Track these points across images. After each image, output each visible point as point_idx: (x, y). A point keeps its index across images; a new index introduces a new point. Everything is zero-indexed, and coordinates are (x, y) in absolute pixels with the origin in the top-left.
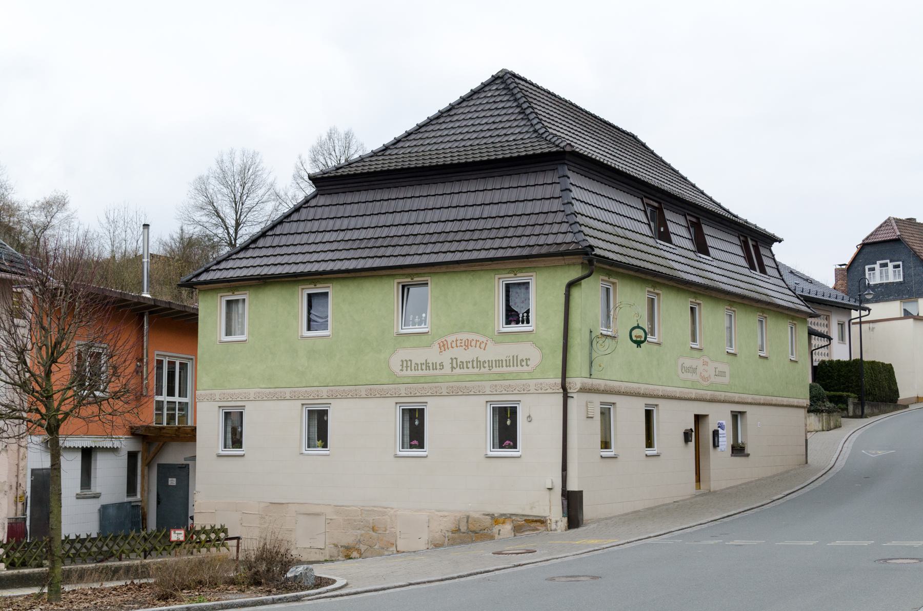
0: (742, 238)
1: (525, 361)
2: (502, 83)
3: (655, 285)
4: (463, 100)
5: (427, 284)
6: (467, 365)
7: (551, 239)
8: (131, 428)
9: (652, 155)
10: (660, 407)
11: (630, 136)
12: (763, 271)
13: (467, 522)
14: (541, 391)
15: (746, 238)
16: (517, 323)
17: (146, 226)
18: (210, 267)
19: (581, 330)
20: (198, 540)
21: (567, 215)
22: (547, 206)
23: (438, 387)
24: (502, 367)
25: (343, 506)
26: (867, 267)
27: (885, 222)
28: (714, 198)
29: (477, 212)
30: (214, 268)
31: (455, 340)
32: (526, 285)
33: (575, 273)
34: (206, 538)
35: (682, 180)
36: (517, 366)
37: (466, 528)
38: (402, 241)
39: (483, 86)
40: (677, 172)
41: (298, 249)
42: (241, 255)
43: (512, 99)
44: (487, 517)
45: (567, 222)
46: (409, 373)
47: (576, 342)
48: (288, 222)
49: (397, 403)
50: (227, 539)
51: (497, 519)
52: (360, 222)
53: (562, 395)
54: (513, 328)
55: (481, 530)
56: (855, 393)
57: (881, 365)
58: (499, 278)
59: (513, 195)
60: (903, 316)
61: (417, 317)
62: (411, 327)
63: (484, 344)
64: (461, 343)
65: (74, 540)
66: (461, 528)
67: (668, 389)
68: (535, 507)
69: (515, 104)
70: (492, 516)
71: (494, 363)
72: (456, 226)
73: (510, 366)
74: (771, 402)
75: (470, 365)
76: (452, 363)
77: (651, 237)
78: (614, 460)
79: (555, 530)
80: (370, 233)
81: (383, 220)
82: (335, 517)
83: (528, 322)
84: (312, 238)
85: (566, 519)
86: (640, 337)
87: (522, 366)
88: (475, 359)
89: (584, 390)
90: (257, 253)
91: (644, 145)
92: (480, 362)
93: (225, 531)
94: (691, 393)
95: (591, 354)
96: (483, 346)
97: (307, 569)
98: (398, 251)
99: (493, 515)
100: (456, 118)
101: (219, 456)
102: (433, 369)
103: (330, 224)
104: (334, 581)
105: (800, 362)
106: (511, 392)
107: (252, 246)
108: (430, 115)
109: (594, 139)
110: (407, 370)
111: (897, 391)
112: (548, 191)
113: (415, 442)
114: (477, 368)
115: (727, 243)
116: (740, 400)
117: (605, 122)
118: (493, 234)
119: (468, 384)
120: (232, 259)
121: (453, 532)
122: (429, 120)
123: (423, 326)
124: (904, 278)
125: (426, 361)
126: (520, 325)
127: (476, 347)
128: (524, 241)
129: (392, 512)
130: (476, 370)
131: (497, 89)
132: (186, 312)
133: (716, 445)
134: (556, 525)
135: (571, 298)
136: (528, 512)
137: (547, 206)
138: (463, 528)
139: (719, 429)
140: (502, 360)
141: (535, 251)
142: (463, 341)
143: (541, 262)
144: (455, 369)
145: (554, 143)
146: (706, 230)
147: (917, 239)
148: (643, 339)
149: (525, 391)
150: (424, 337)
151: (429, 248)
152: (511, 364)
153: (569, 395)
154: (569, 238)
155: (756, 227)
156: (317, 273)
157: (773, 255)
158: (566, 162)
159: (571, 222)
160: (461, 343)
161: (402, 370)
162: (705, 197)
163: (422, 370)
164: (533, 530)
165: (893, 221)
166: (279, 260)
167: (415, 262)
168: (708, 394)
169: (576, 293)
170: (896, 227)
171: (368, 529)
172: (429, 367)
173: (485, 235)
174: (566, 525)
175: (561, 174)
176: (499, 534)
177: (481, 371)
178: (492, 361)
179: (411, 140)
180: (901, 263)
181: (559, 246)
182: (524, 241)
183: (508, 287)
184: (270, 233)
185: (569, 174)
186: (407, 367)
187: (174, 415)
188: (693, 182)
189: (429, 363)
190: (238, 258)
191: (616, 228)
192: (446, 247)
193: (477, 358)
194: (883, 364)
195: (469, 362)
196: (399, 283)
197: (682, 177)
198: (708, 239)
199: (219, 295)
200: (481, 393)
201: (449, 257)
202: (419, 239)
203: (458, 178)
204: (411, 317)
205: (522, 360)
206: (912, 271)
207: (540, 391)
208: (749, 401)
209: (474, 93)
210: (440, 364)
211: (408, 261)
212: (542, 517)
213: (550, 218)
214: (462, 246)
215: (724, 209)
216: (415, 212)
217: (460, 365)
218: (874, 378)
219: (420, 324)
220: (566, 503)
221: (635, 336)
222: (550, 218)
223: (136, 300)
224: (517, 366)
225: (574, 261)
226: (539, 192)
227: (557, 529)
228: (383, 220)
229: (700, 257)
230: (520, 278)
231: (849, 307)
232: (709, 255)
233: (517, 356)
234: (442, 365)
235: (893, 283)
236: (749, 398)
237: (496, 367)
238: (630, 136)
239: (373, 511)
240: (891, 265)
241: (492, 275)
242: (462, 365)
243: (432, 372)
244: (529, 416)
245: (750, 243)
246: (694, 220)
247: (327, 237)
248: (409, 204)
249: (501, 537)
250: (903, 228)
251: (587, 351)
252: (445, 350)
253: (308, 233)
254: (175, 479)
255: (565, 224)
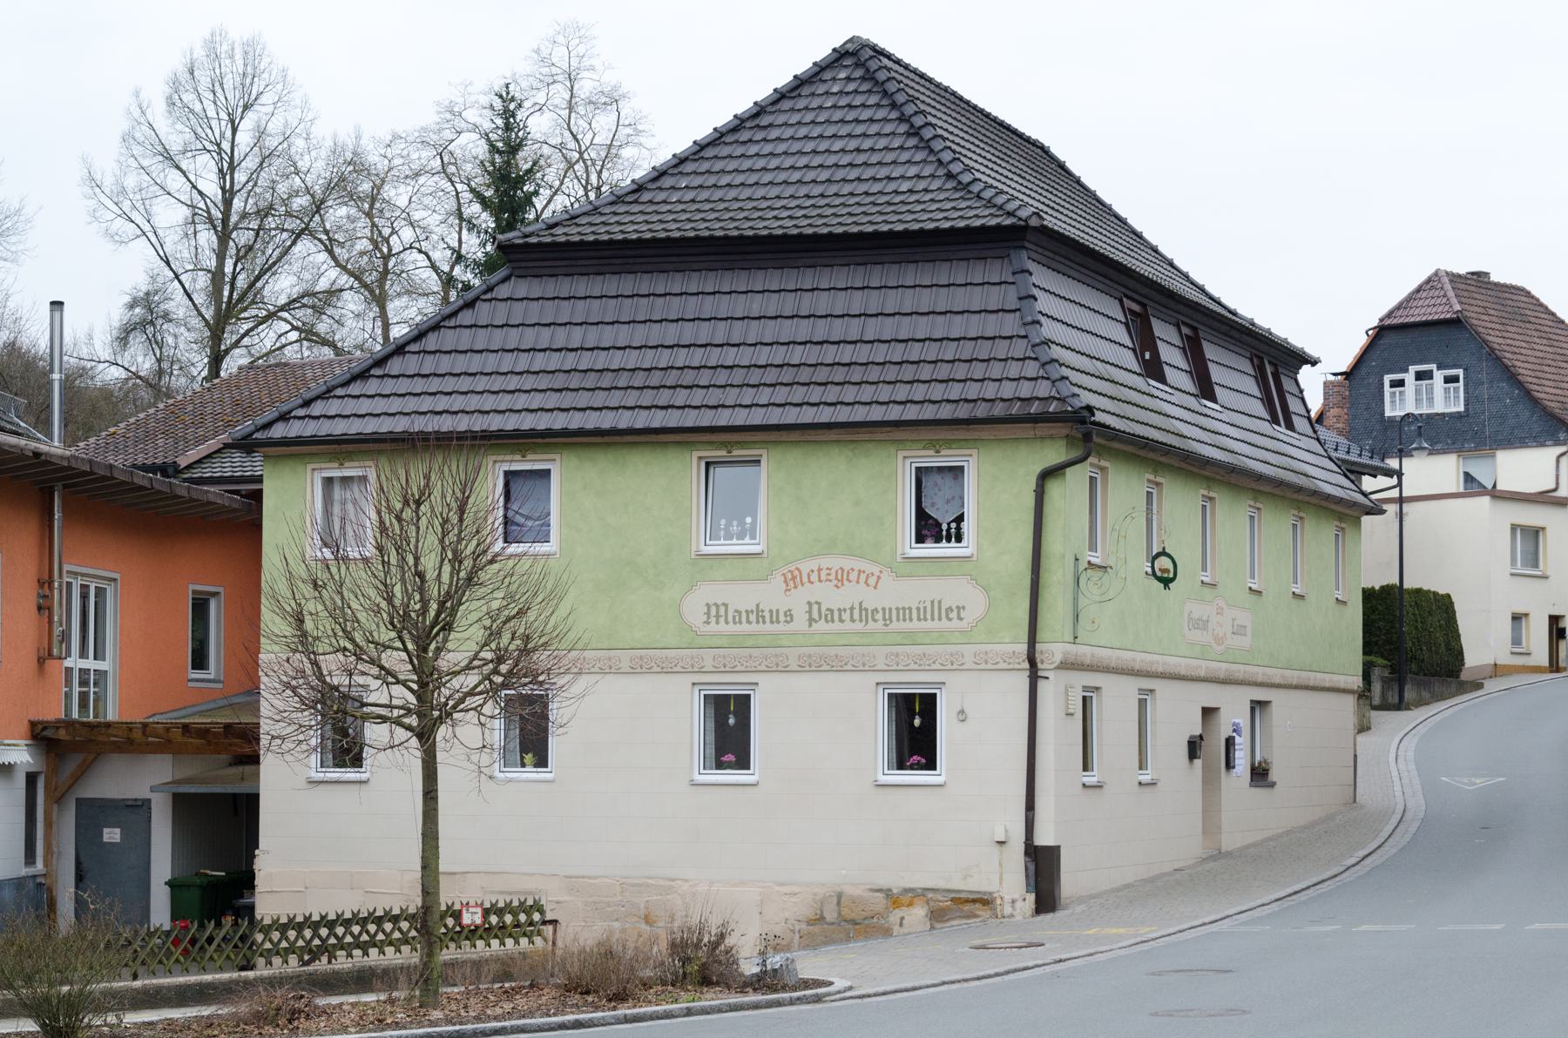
0: (1185, 330)
1: (955, 611)
2: (857, 65)
3: (1157, 467)
4: (781, 96)
5: (759, 461)
6: (840, 615)
7: (1007, 390)
8: (33, 724)
9: (1078, 187)
10: (1158, 694)
11: (1038, 147)
12: (1290, 426)
13: (839, 903)
14: (985, 665)
15: (1261, 359)
16: (938, 540)
17: (57, 305)
18: (291, 411)
19: (1064, 557)
20: (487, 926)
21: (1033, 346)
22: (992, 325)
23: (781, 655)
24: (911, 620)
25: (583, 877)
26: (1387, 379)
27: (1429, 280)
28: (1192, 275)
29: (853, 329)
30: (301, 412)
31: (816, 569)
32: (957, 472)
33: (1054, 454)
34: (498, 923)
35: (1135, 237)
36: (940, 619)
37: (835, 915)
38: (705, 378)
39: (818, 69)
40: (1123, 221)
41: (481, 383)
42: (355, 389)
43: (884, 102)
44: (878, 894)
45: (1036, 359)
46: (722, 627)
47: (1055, 578)
48: (449, 327)
49: (694, 684)
50: (544, 923)
51: (897, 899)
52: (608, 336)
53: (1028, 673)
54: (930, 549)
55: (865, 919)
56: (1382, 656)
57: (1432, 596)
58: (905, 457)
59: (925, 300)
60: (1462, 490)
61: (735, 523)
62: (722, 542)
63: (875, 578)
64: (829, 574)
65: (319, 922)
66: (825, 915)
67: (1173, 660)
68: (971, 876)
69: (894, 115)
70: (888, 893)
71: (894, 613)
72: (812, 354)
73: (926, 619)
74: (1322, 684)
75: (846, 616)
76: (810, 612)
77: (1139, 374)
78: (1097, 790)
79: (1012, 916)
80: (632, 359)
81: (655, 334)
82: (566, 898)
83: (959, 539)
84: (507, 362)
85: (1031, 897)
86: (1167, 571)
87: (950, 620)
88: (857, 606)
89: (1067, 665)
90: (389, 386)
91: (1062, 166)
92: (866, 610)
93: (541, 911)
94: (1200, 667)
95: (1076, 600)
96: (872, 581)
97: (787, 959)
98: (698, 397)
99: (890, 890)
100: (774, 134)
101: (312, 782)
102: (772, 622)
103: (545, 337)
104: (831, 983)
105: (1349, 603)
106: (927, 668)
107: (377, 372)
108: (719, 124)
109: (1014, 173)
110: (717, 623)
111: (1461, 653)
112: (994, 297)
113: (730, 758)
114: (861, 621)
115: (1086, 311)
116: (1266, 680)
117: (1002, 124)
118: (891, 373)
119: (841, 651)
120: (335, 396)
121: (810, 923)
122: (718, 135)
123: (747, 540)
124: (1467, 405)
125: (758, 606)
126: (944, 543)
127: (858, 582)
128: (955, 391)
129: (686, 887)
130: (859, 626)
131: (848, 79)
132: (133, 483)
133: (1229, 765)
134: (1013, 907)
135: (1047, 498)
136: (957, 884)
137: (992, 325)
138: (830, 916)
139: (1234, 734)
140: (910, 609)
141: (981, 411)
142: (833, 572)
143: (986, 432)
144: (816, 622)
145: (1001, 208)
146: (1210, 351)
147: (1494, 319)
148: (1171, 575)
149: (955, 666)
150: (752, 562)
151: (764, 396)
152: (929, 616)
153: (1040, 673)
154: (1043, 389)
155: (1271, 334)
156: (533, 434)
157: (1301, 391)
158: (1027, 245)
159: (1044, 359)
160: (829, 574)
161: (708, 623)
162: (1176, 272)
163: (749, 622)
164: (968, 917)
165: (1446, 280)
166: (442, 403)
167: (739, 422)
168: (1221, 669)
169: (1054, 489)
170: (1451, 294)
171: (636, 919)
172: (763, 617)
173: (874, 374)
174: (1034, 907)
175: (1017, 267)
176: (901, 925)
177: (868, 626)
178: (890, 609)
179: (688, 174)
180: (1460, 372)
181: (1026, 402)
182: (955, 391)
183: (921, 473)
184: (414, 347)
185: (1031, 266)
186: (718, 616)
187: (88, 692)
188: (1154, 242)
189: (763, 611)
190: (349, 396)
191: (1094, 361)
192: (798, 394)
193: (861, 603)
194: (1435, 594)
195: (845, 610)
196: (700, 458)
197: (1134, 232)
198: (1213, 368)
199: (310, 467)
200: (867, 668)
201: (808, 415)
202: (738, 376)
203: (810, 261)
204: (723, 522)
205: (950, 609)
206: (1485, 392)
207: (983, 666)
208: (1277, 680)
209: (800, 83)
210: (785, 613)
211: (723, 418)
212: (985, 893)
213: (1001, 349)
214: (832, 394)
215: (1212, 298)
216: (707, 323)
217: (826, 615)
218: (1420, 625)
219: (741, 536)
220: (1032, 867)
221: (1160, 570)
222: (1001, 349)
223: (66, 464)
224: (940, 619)
225: (1054, 432)
226: (975, 299)
227: (1014, 913)
228: (655, 334)
229: (1205, 406)
230: (947, 459)
231: (1360, 470)
232: (1215, 401)
233: (940, 602)
234: (789, 616)
235: (1443, 415)
236: (1276, 675)
237: (898, 620)
238: (1038, 147)
239: (648, 886)
240: (1439, 376)
241: (892, 450)
242: (830, 615)
243: (768, 627)
244: (962, 712)
245: (1269, 369)
246: (1136, 308)
247: (539, 362)
248: (709, 306)
249: (906, 931)
250: (1465, 294)
251: (1070, 596)
252: (795, 587)
253: (497, 351)
254: (118, 831)
255: (1032, 362)
